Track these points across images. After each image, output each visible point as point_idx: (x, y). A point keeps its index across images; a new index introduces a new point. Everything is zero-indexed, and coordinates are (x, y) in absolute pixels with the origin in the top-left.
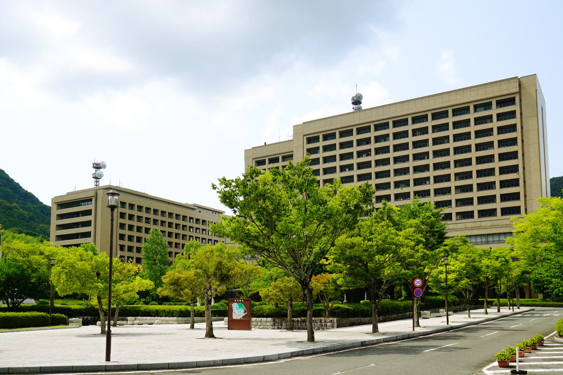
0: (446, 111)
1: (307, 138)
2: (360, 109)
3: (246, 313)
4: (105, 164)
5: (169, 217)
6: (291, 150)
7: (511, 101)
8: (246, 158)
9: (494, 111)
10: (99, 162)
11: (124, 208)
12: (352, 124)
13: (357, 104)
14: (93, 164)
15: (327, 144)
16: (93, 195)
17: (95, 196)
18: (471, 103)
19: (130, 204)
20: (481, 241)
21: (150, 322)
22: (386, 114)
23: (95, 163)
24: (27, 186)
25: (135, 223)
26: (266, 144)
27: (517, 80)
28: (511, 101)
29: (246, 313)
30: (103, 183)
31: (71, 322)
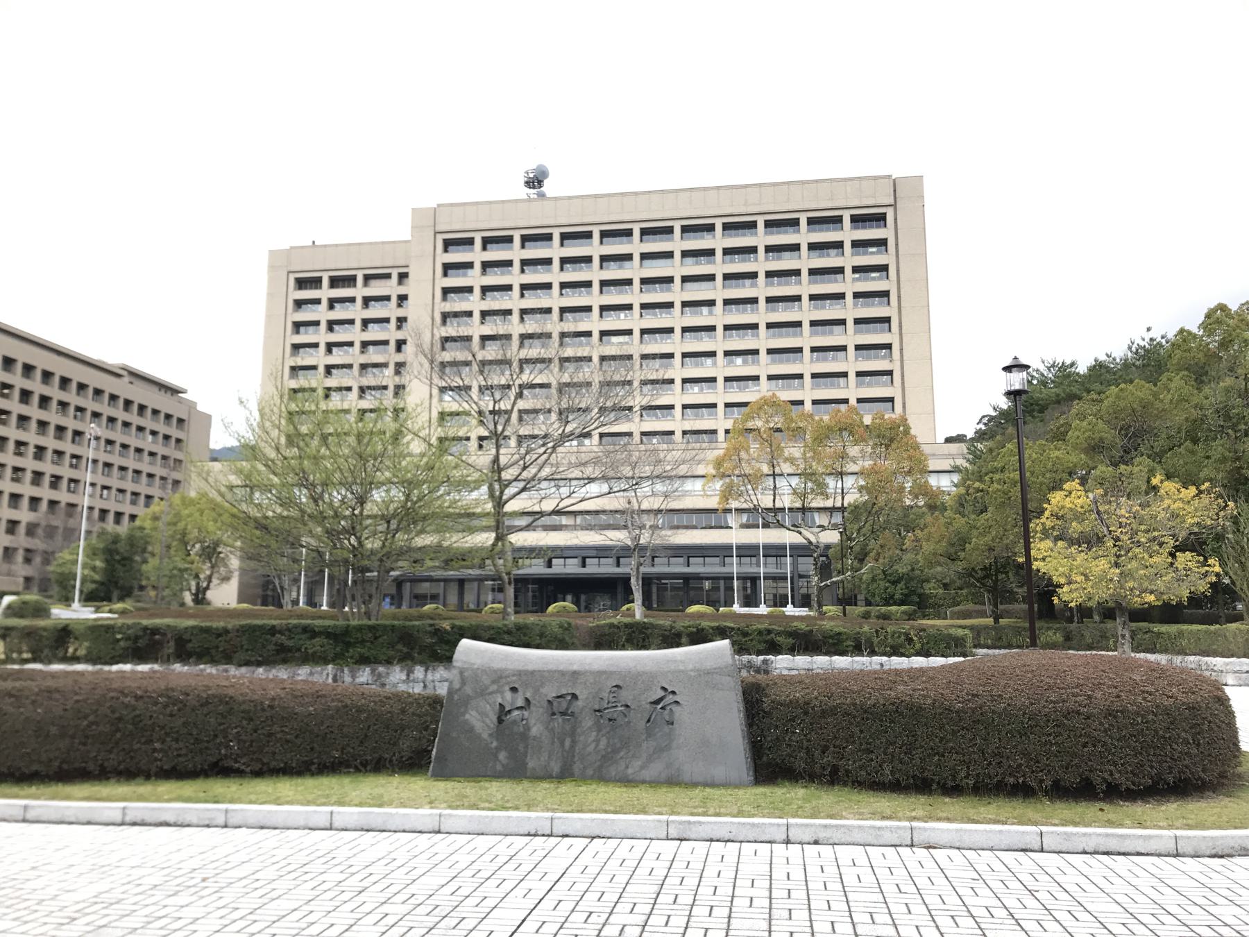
2: (542, 196)
5: (18, 428)
7: (880, 219)
8: (272, 268)
12: (552, 223)
28: (880, 219)
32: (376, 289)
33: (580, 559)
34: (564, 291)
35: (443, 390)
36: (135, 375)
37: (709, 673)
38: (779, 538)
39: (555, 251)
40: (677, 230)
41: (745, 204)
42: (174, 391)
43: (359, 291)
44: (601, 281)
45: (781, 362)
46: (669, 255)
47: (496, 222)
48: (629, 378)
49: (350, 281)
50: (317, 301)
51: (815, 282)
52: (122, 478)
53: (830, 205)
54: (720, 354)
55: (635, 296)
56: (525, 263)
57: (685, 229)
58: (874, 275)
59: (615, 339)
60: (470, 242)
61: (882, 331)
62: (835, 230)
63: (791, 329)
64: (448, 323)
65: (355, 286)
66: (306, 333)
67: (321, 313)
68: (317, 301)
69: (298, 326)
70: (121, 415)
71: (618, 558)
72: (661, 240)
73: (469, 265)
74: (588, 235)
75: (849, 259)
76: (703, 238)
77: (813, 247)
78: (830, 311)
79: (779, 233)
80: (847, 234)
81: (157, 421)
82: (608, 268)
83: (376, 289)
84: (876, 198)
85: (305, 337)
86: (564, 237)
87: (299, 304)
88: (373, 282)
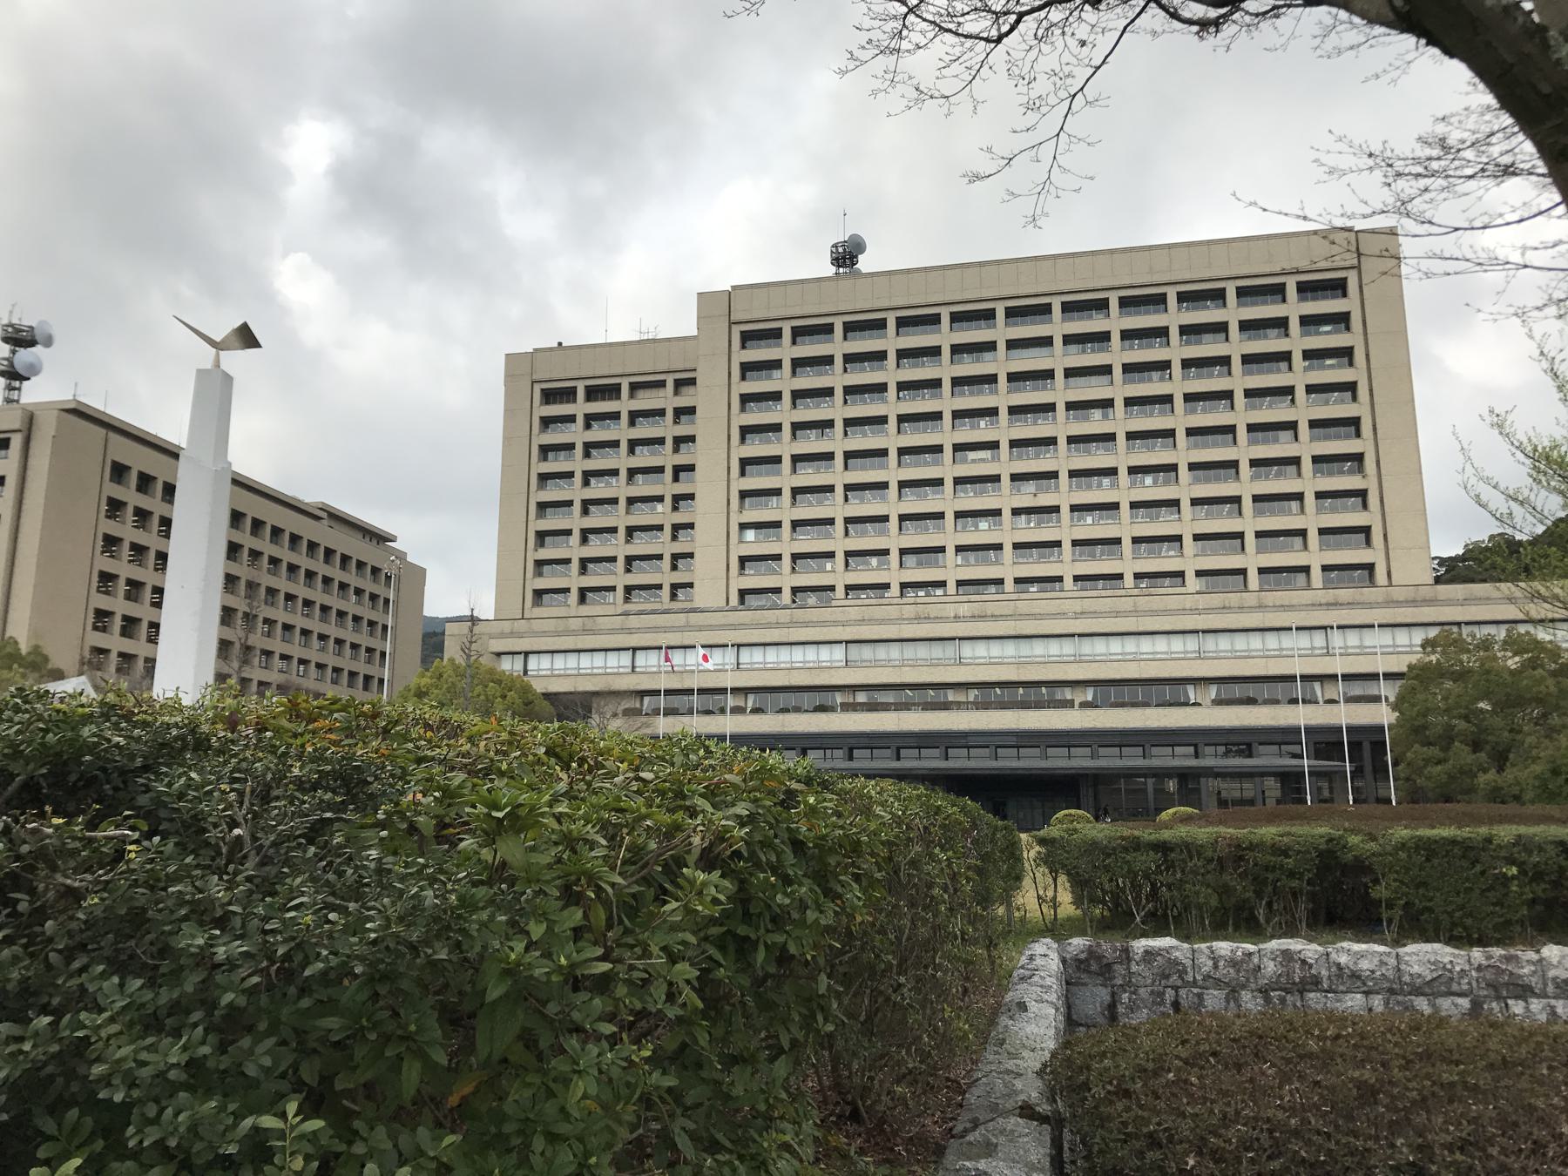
6: (689, 366)
7: (1338, 287)
8: (511, 376)
9: (1174, 317)
12: (886, 304)
16: (17, 426)
17: (25, 428)
18: (1230, 282)
20: (1407, 643)
28: (1338, 287)
32: (646, 401)
33: (846, 749)
34: (901, 394)
35: (743, 527)
36: (337, 518)
38: (1273, 718)
39: (891, 342)
40: (945, 320)
42: (379, 538)
43: (624, 405)
45: (1207, 480)
46: (1047, 342)
47: (811, 307)
49: (612, 391)
50: (571, 419)
51: (1251, 373)
52: (322, 649)
53: (1207, 275)
54: (1123, 472)
55: (1002, 397)
56: (849, 358)
58: (1329, 362)
59: (972, 455)
60: (777, 334)
61: (1225, 445)
62: (1156, 312)
63: (1219, 437)
64: (748, 441)
65: (575, 401)
66: (556, 460)
67: (575, 434)
68: (571, 419)
69: (545, 450)
70: (321, 569)
71: (898, 749)
72: (871, 338)
73: (776, 364)
75: (1176, 351)
76: (1091, 317)
77: (1068, 340)
79: (1139, 313)
80: (1115, 322)
81: (363, 576)
83: (646, 401)
84: (1321, 261)
86: (902, 323)
87: (546, 422)
88: (641, 393)
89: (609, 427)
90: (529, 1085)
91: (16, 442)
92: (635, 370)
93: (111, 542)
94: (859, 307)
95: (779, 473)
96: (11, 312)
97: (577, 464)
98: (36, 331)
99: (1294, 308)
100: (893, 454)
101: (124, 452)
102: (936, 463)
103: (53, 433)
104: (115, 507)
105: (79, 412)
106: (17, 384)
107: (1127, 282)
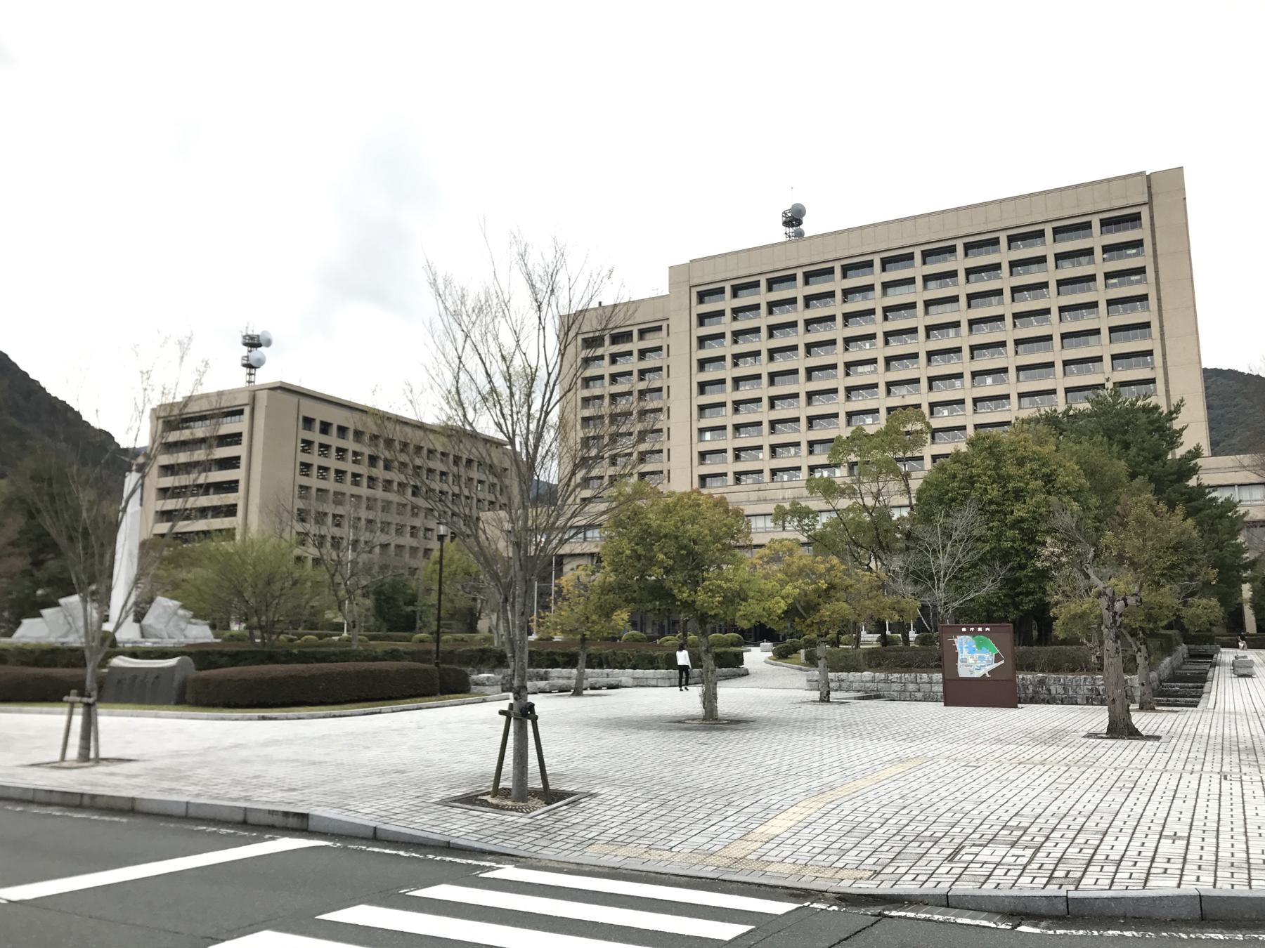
0: (1040, 231)
1: (698, 292)
2: (800, 234)
3: (1002, 662)
4: (269, 337)
7: (1133, 219)
10: (257, 332)
11: (310, 429)
13: (793, 226)
14: (244, 337)
15: (740, 305)
16: (246, 401)
17: (251, 403)
19: (322, 423)
21: (612, 681)
22: (869, 244)
23: (249, 336)
24: (55, 388)
25: (332, 463)
26: (603, 305)
27: (1145, 178)
28: (1133, 219)
29: (1002, 662)
30: (264, 377)
31: (477, 684)
37: (208, 653)
41: (986, 222)
44: (1012, 288)
47: (779, 264)
48: (632, 430)
49: (627, 337)
53: (1028, 221)
57: (1104, 223)
58: (1133, 278)
59: (860, 369)
60: (870, 264)
73: (721, 313)
74: (995, 242)
78: (1034, 329)
82: (852, 301)
84: (1119, 202)
85: (711, 374)
88: (648, 336)
89: (788, 334)
90: (139, 588)
91: (247, 410)
92: (642, 321)
93: (306, 467)
94: (815, 260)
95: (797, 382)
96: (247, 328)
97: (839, 356)
98: (261, 339)
99: (1097, 239)
100: (1011, 345)
101: (310, 409)
102: (1047, 350)
103: (265, 404)
104: (307, 444)
105: (284, 389)
106: (253, 371)
107: (969, 231)
